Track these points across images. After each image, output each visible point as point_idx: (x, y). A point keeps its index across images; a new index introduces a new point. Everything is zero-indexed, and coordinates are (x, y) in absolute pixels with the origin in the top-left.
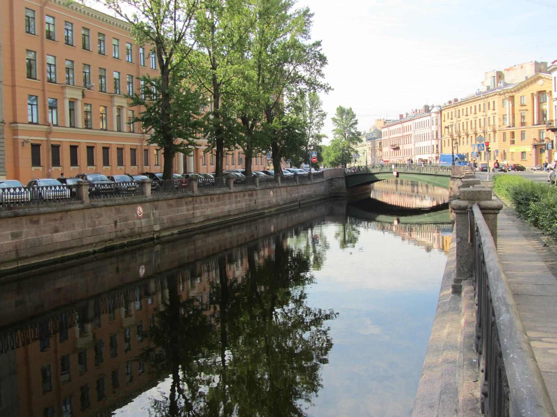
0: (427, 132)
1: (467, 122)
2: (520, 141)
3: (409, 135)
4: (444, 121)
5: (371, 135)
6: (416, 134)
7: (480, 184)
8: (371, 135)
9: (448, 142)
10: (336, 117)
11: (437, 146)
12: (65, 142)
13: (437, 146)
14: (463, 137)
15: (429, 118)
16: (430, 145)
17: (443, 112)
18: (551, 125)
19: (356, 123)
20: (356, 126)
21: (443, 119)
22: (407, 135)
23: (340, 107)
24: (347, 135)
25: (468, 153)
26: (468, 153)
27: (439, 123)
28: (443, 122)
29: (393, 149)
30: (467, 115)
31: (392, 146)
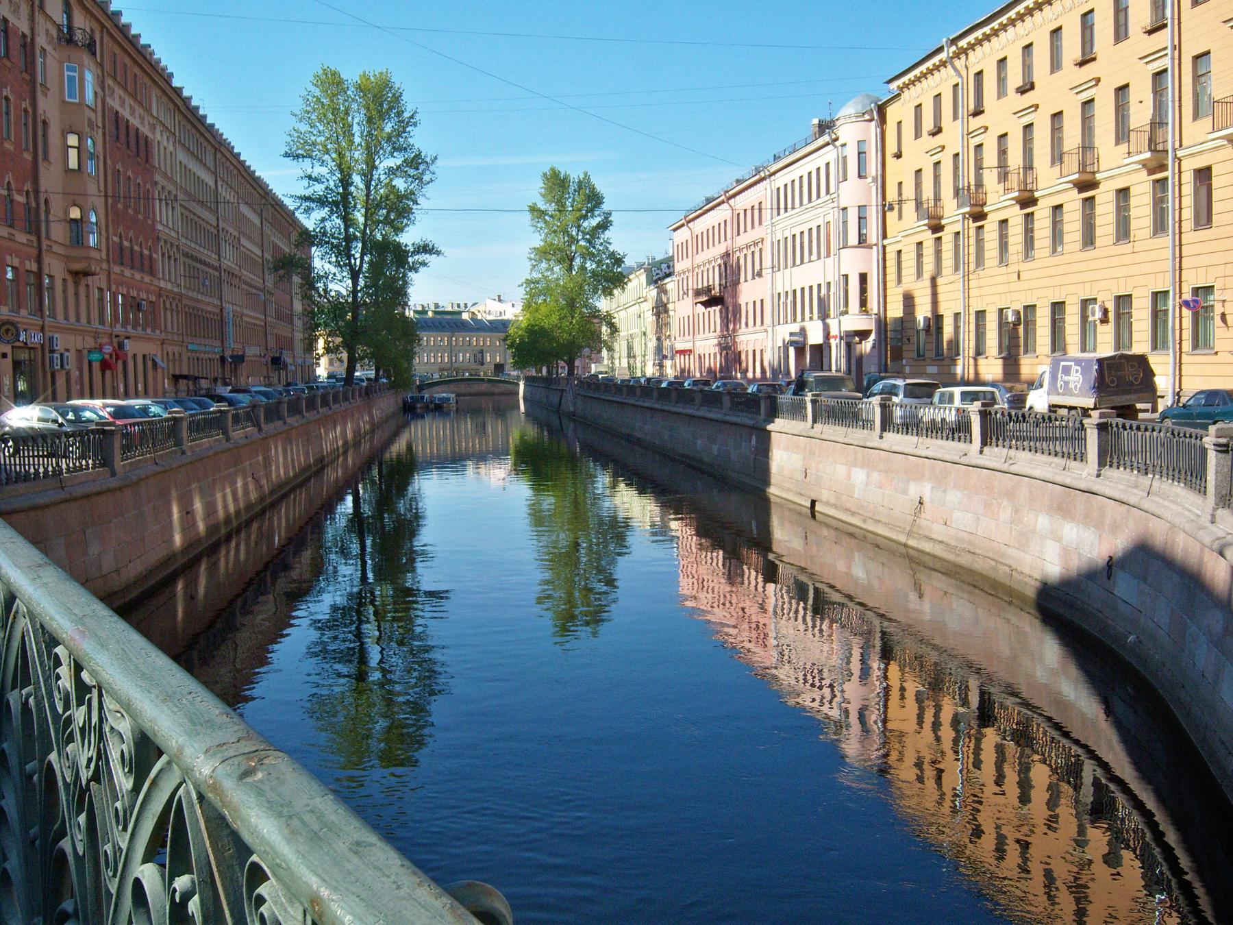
0: (820, 222)
1: (1028, 128)
2: (1094, 478)
3: (755, 244)
4: (898, 156)
5: (664, 266)
6: (779, 236)
7: (1196, 116)
8: (664, 266)
9: (913, 255)
10: (542, 205)
11: (863, 278)
12: (1027, 451)
13: (863, 278)
14: (1002, 215)
15: (829, 155)
16: (832, 277)
17: (892, 113)
18: (362, 791)
19: (604, 225)
20: (607, 234)
21: (891, 147)
22: (748, 247)
23: (552, 169)
24: (577, 262)
25: (1030, 309)
26: (1030, 309)
27: (873, 167)
28: (890, 160)
29: (703, 303)
30: (1027, 87)
31: (698, 293)
